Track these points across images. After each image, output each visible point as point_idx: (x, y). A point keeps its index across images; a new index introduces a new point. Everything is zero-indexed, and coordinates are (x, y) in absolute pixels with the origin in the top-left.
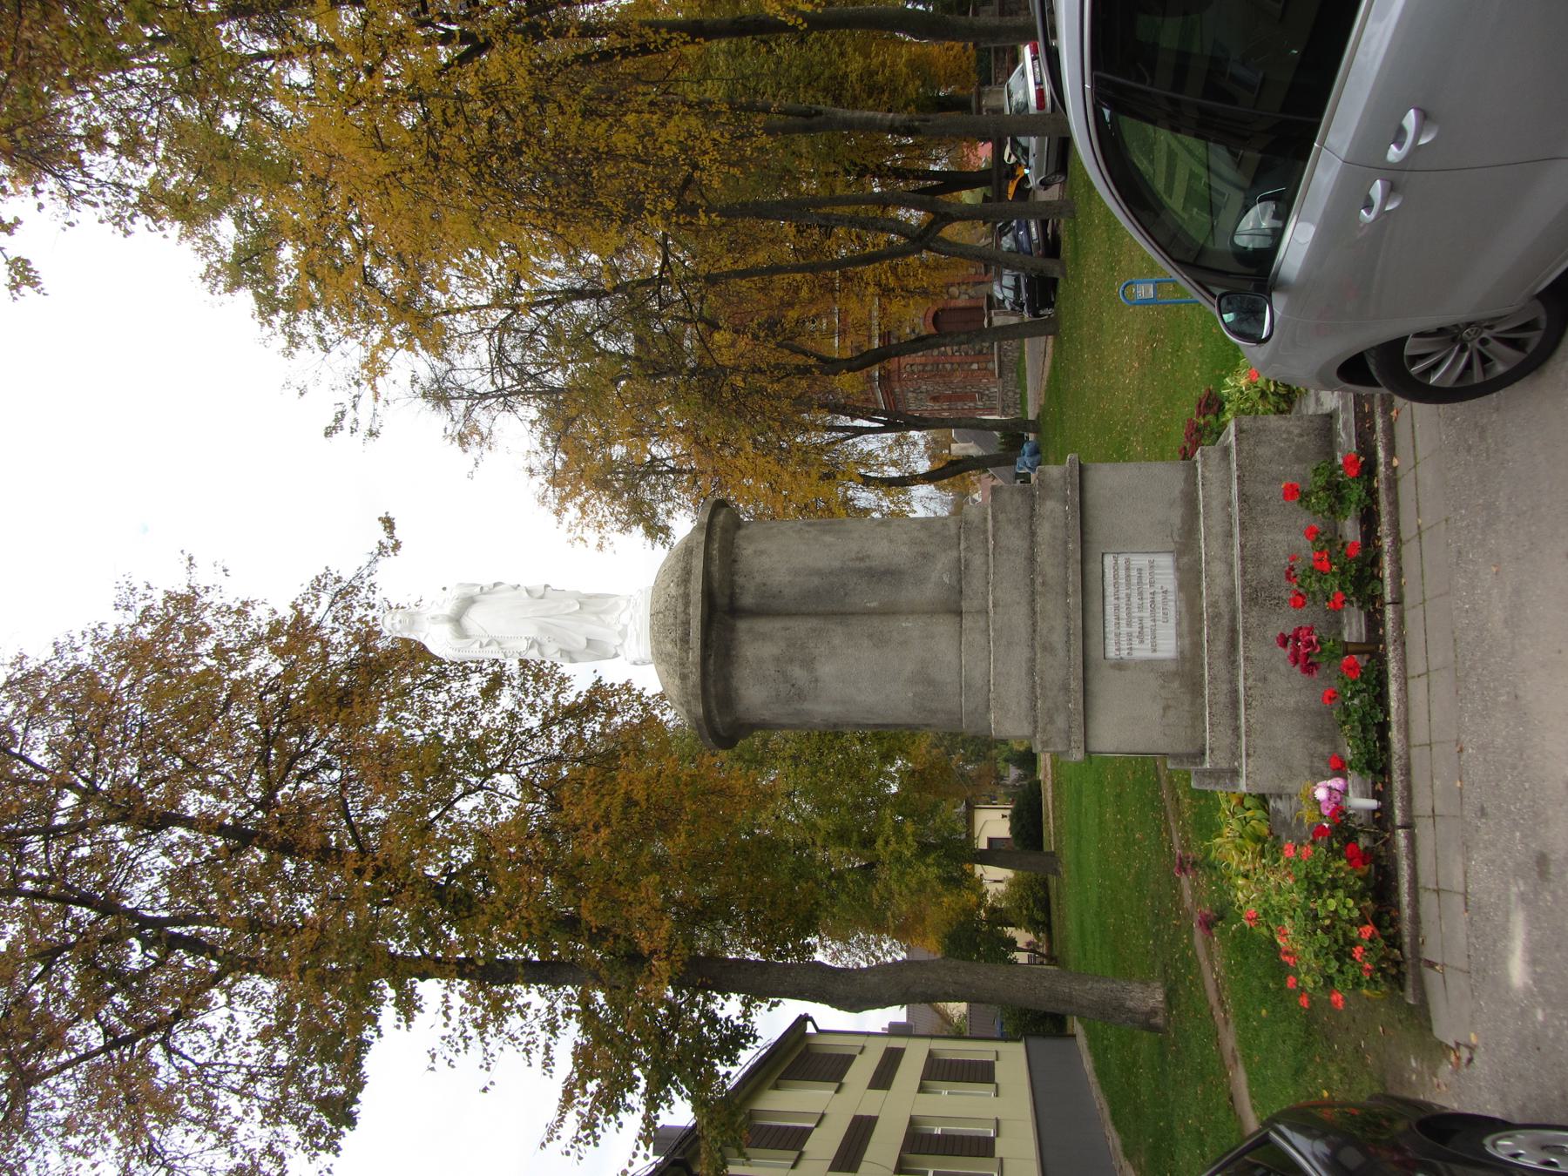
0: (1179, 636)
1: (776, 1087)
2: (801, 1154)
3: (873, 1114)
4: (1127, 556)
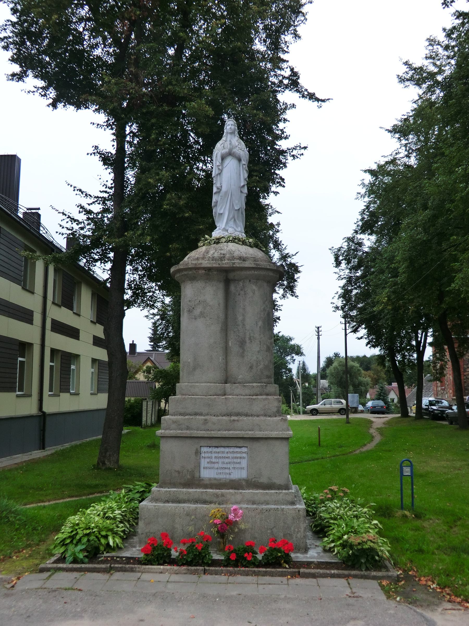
0: (210, 479)
1: (93, 295)
2: (60, 306)
3: (80, 338)
4: (246, 458)
